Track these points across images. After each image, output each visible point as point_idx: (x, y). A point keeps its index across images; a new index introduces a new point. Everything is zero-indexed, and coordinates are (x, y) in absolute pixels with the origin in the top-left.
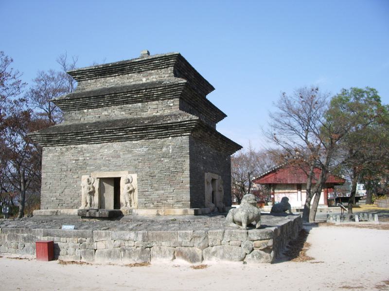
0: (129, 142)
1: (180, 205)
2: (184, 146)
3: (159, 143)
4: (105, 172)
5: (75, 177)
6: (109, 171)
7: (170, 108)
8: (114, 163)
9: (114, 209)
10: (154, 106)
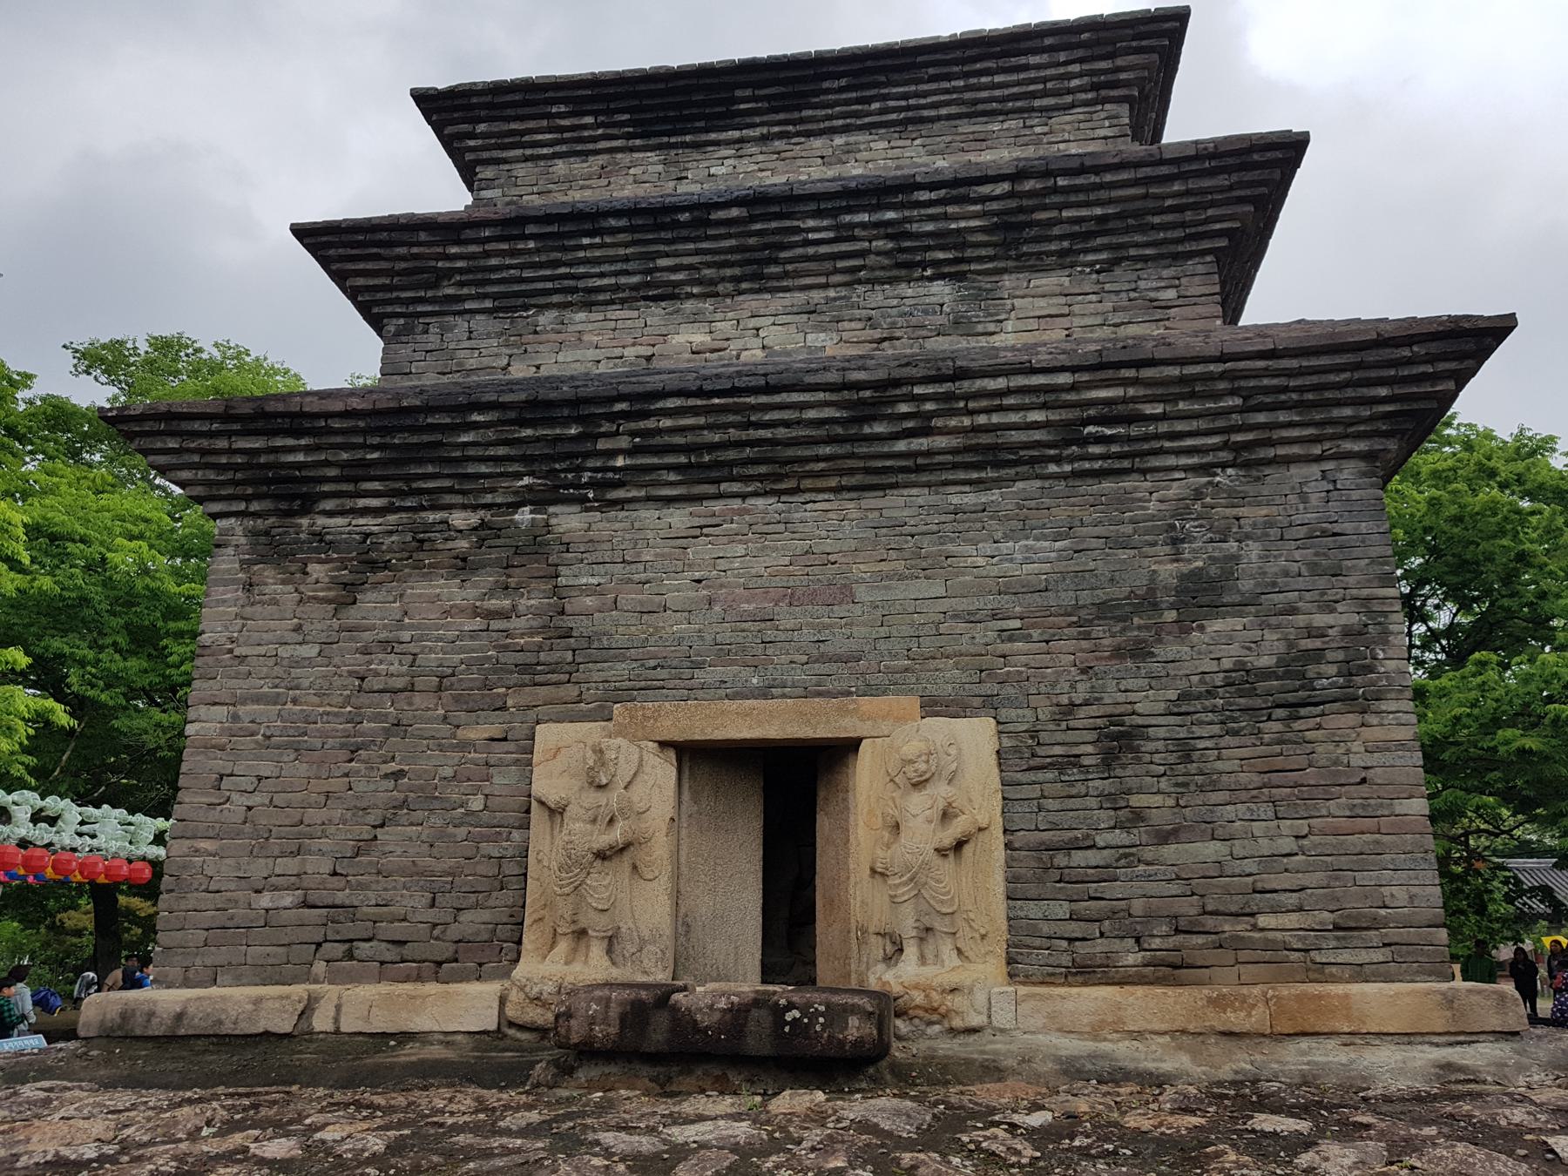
0: (922, 496)
1: (1363, 956)
2: (1347, 527)
3: (1153, 507)
4: (734, 705)
5: (477, 732)
6: (764, 693)
7: (1158, 314)
8: (808, 635)
9: (764, 982)
10: (1042, 302)
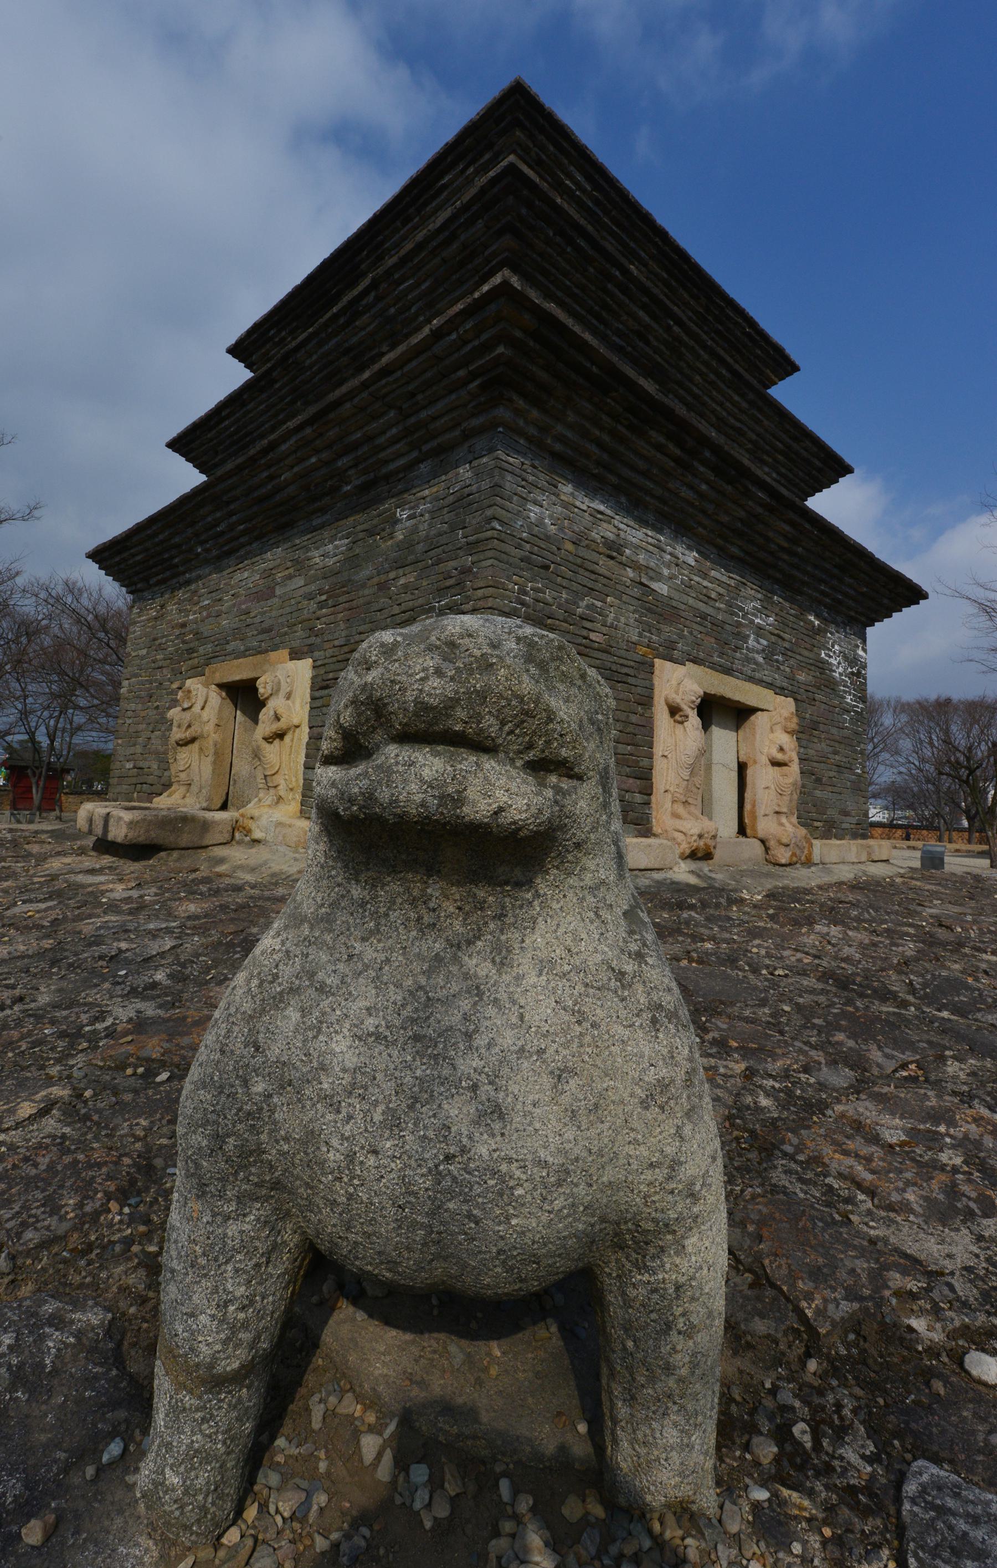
8: (258, 620)
